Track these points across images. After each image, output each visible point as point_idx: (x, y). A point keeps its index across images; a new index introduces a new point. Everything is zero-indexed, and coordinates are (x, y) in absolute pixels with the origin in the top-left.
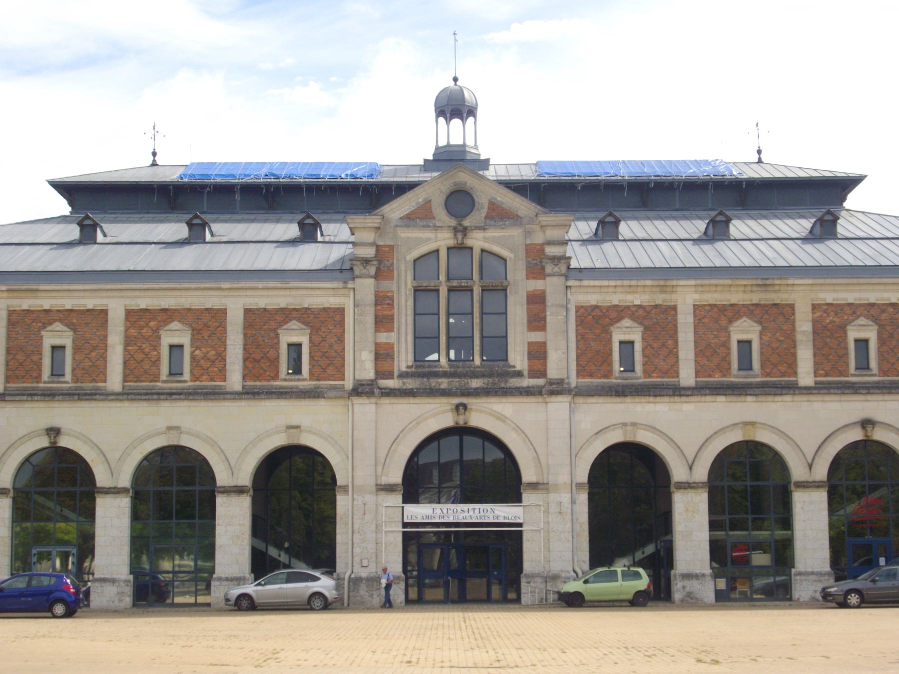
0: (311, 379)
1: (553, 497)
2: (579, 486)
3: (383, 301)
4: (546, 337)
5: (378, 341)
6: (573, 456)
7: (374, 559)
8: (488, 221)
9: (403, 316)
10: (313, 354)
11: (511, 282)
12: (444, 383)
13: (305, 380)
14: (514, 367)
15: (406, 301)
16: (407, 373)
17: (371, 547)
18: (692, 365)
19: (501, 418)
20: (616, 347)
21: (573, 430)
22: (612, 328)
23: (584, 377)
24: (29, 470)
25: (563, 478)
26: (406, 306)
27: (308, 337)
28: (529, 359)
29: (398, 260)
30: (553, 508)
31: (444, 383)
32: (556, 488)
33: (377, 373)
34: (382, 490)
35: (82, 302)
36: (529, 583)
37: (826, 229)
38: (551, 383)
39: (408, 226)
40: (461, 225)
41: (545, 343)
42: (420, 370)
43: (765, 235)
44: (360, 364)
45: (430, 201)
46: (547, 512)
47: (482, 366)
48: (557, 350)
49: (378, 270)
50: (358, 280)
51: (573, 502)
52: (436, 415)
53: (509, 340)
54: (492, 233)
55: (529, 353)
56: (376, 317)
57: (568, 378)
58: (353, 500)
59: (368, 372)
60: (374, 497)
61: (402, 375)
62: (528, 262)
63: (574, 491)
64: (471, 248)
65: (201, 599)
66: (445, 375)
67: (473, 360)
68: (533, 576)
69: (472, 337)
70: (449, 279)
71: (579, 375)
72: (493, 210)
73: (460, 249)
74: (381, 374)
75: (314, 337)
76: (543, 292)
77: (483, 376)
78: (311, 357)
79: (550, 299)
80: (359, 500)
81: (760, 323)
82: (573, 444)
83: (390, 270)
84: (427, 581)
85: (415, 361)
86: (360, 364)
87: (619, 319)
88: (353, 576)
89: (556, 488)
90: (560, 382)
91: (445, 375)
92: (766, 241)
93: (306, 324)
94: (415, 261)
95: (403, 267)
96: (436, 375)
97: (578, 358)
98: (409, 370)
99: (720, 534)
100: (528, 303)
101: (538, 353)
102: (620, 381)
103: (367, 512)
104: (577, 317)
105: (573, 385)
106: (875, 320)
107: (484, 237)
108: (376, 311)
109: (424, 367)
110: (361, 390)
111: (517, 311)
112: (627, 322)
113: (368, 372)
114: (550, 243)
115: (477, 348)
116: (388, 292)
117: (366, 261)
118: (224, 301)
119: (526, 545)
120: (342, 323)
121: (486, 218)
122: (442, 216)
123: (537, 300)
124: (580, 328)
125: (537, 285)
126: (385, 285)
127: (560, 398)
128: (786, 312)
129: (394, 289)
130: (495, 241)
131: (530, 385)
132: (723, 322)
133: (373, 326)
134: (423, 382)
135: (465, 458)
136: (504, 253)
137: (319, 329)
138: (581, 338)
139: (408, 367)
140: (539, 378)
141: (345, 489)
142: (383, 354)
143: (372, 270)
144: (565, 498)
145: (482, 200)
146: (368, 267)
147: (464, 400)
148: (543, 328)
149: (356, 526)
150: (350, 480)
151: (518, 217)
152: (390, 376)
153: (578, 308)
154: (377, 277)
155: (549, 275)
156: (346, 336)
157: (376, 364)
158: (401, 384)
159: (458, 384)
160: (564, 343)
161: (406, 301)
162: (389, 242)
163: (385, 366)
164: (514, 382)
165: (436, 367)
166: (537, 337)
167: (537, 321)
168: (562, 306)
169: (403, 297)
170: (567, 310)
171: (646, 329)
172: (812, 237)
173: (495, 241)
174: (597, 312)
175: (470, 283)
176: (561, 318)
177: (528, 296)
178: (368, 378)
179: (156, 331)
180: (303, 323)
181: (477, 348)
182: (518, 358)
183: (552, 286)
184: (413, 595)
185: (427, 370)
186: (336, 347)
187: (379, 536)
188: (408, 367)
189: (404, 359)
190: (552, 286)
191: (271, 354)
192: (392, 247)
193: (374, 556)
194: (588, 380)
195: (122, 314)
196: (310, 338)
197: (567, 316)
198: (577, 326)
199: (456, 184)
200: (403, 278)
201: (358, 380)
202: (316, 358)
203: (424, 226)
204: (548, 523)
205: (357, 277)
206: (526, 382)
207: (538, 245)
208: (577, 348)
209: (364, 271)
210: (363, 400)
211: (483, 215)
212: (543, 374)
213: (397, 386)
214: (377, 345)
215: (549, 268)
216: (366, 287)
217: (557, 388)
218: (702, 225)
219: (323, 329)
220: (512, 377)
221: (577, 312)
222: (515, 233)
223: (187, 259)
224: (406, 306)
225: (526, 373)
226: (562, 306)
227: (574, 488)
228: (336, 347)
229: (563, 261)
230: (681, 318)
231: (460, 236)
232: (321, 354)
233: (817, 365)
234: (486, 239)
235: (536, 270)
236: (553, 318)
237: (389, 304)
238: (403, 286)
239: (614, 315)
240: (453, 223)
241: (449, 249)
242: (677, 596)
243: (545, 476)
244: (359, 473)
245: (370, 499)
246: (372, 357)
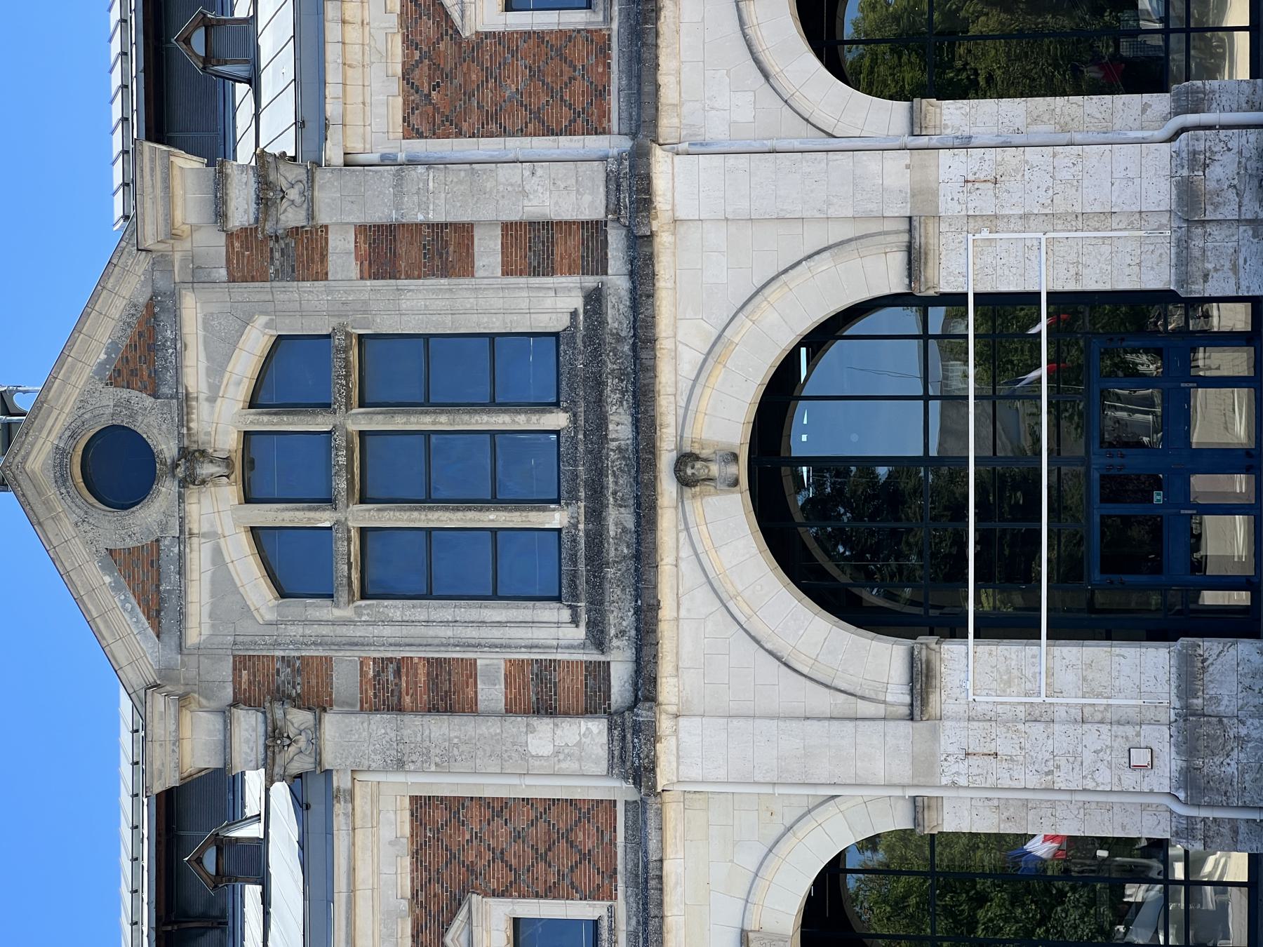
0: (612, 896)
1: (948, 205)
2: (915, 126)
3: (389, 690)
4: (491, 223)
5: (501, 706)
6: (829, 142)
7: (1130, 731)
8: (165, 390)
9: (431, 631)
10: (541, 890)
11: (335, 322)
13: (611, 909)
14: (574, 314)
15: (392, 622)
16: (591, 625)
17: (1095, 737)
19: (716, 347)
21: (757, 146)
22: (466, 34)
23: (604, 114)
25: (892, 175)
26: (403, 622)
27: (492, 901)
28: (550, 271)
29: (276, 644)
30: (984, 202)
31: (618, 518)
32: (924, 194)
33: (589, 711)
34: (924, 702)
36: (1206, 277)
38: (614, 208)
39: (181, 617)
40: (175, 465)
41: (507, 227)
42: (582, 585)
44: (565, 758)
45: (111, 552)
46: (993, 221)
47: (571, 410)
48: (525, 194)
49: (300, 702)
50: (329, 761)
51: (965, 144)
52: (713, 551)
53: (496, 326)
54: (195, 376)
55: (535, 272)
56: (433, 709)
57: (604, 159)
58: (954, 785)
59: (589, 736)
60: (948, 724)
61: (598, 638)
62: (280, 275)
63: (934, 141)
66: (596, 514)
67: (557, 432)
68: (1183, 259)
70: (328, 501)
71: (599, 130)
72: (133, 373)
74: (594, 701)
75: (493, 884)
76: (363, 230)
77: (598, 403)
78: (550, 892)
79: (381, 213)
80: (954, 770)
82: (797, 145)
83: (300, 666)
85: (558, 599)
86: (565, 758)
88: (1182, 795)
89: (924, 194)
90: (614, 182)
91: (596, 514)
93: (456, 903)
94: (283, 595)
95: (296, 631)
96: (596, 540)
97: (551, 132)
98: (584, 618)
101: (534, 246)
102: (616, 8)
103: (991, 748)
104: (435, 135)
105: (625, 144)
107: (208, 399)
108: (414, 711)
109: (574, 576)
110: (635, 758)
113: (589, 736)
114: (220, 214)
115: (522, 421)
116: (363, 674)
117: (275, 737)
119: (1091, 283)
120: (455, 806)
121: (155, 395)
122: (148, 517)
123: (386, 250)
124: (465, 126)
125: (342, 249)
126: (345, 680)
127: (661, 183)
129: (355, 655)
130: (218, 367)
131: (625, 269)
133: (457, 720)
134: (612, 577)
135: (849, 876)
137: (471, 869)
138: (494, 123)
139: (575, 621)
140: (605, 243)
141: (918, 806)
142: (539, 693)
143: (299, 718)
144: (951, 166)
145: (109, 406)
146: (292, 732)
147: (666, 460)
148: (465, 231)
149: (1033, 781)
150: (898, 792)
151: (150, 304)
152: (599, 672)
153: (411, 131)
154: (319, 705)
155: (311, 215)
156: (488, 793)
157: (566, 714)
158: (623, 643)
159: (620, 475)
160: (504, 171)
161: (392, 622)
162: (225, 670)
163: (571, 687)
164: (616, 315)
165: (574, 540)
167: (444, 249)
168: (399, 178)
169: (377, 631)
170: (412, 162)
173: (218, 367)
174: (421, 76)
175: (339, 440)
176: (433, 179)
177: (376, 277)
178: (604, 738)
180: (453, 915)
181: (522, 421)
182: (551, 303)
183: (342, 210)
185: (582, 567)
186: (521, 823)
187: (1061, 713)
188: (575, 621)
189: (552, 631)
190: (342, 210)
192: (240, 663)
193: (1120, 730)
194: (614, 103)
196: (495, 894)
197: (429, 164)
198: (459, 134)
199: (62, 478)
200: (325, 630)
201: (611, 767)
202: (552, 879)
203: (181, 572)
204: (1025, 217)
205: (319, 762)
206: (617, 281)
207: (230, 244)
208: (522, 132)
209: (302, 741)
210: (666, 753)
211: (149, 401)
212: (595, 229)
213: (629, 654)
214: (511, 710)
215: (291, 216)
216: (344, 736)
217: (632, 189)
219: (471, 856)
220: (603, 323)
221: (420, 135)
224: (403, 622)
225: (591, 281)
226: (399, 178)
227: (923, 141)
228: (521, 823)
229: (272, 177)
231: (206, 469)
232: (542, 865)
235: (302, 253)
236: (435, 202)
237: (398, 673)
238: (349, 631)
239: (428, 27)
240: (166, 489)
241: (248, 500)
243: (888, 226)
244: (878, 769)
245: (952, 737)
246: (544, 725)
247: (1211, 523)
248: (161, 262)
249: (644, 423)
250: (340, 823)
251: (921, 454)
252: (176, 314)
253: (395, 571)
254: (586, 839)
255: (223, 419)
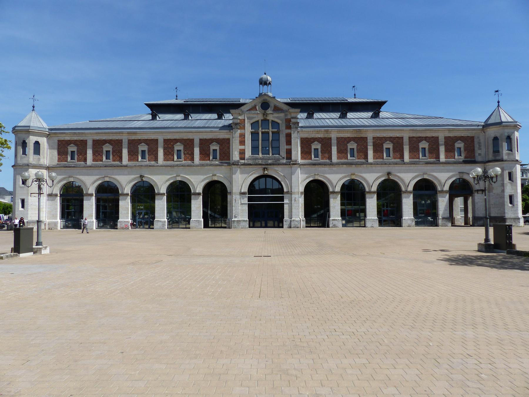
12: (260, 162)
18: (336, 155)
20: (313, 150)
24: (135, 187)
35: (144, 137)
37: (376, 115)
43: (324, 117)
64: (269, 120)
65: (187, 226)
69: (258, 147)
73: (265, 121)
78: (220, 153)
81: (356, 143)
84: (491, 230)
86: (235, 156)
87: (314, 142)
90: (296, 161)
92: (356, 118)
99: (362, 207)
100: (286, 137)
101: (242, 153)
106: (392, 142)
111: (283, 139)
112: (316, 142)
114: (292, 118)
118: (122, 137)
128: (365, 139)
130: (277, 118)
132: (346, 142)
136: (279, 121)
142: (242, 153)
145: (272, 105)
147: (266, 166)
148: (291, 144)
152: (244, 159)
166: (242, 147)
171: (322, 145)
172: (372, 117)
179: (173, 146)
184: (251, 225)
191: (208, 153)
195: (127, 141)
199: (264, 100)
212: (291, 159)
218: (306, 114)
222: (282, 115)
223: (185, 123)
230: (333, 141)
233: (410, 156)
234: (273, 117)
235: (289, 127)
239: (312, 140)
242: (331, 226)
246: (238, 153)
247: (260, 223)
248: (287, 111)
249: (270, 164)
250: (227, 131)
251: (264, 187)
252: (281, 113)
253: (254, 135)
254: (226, 158)
255: (270, 118)
